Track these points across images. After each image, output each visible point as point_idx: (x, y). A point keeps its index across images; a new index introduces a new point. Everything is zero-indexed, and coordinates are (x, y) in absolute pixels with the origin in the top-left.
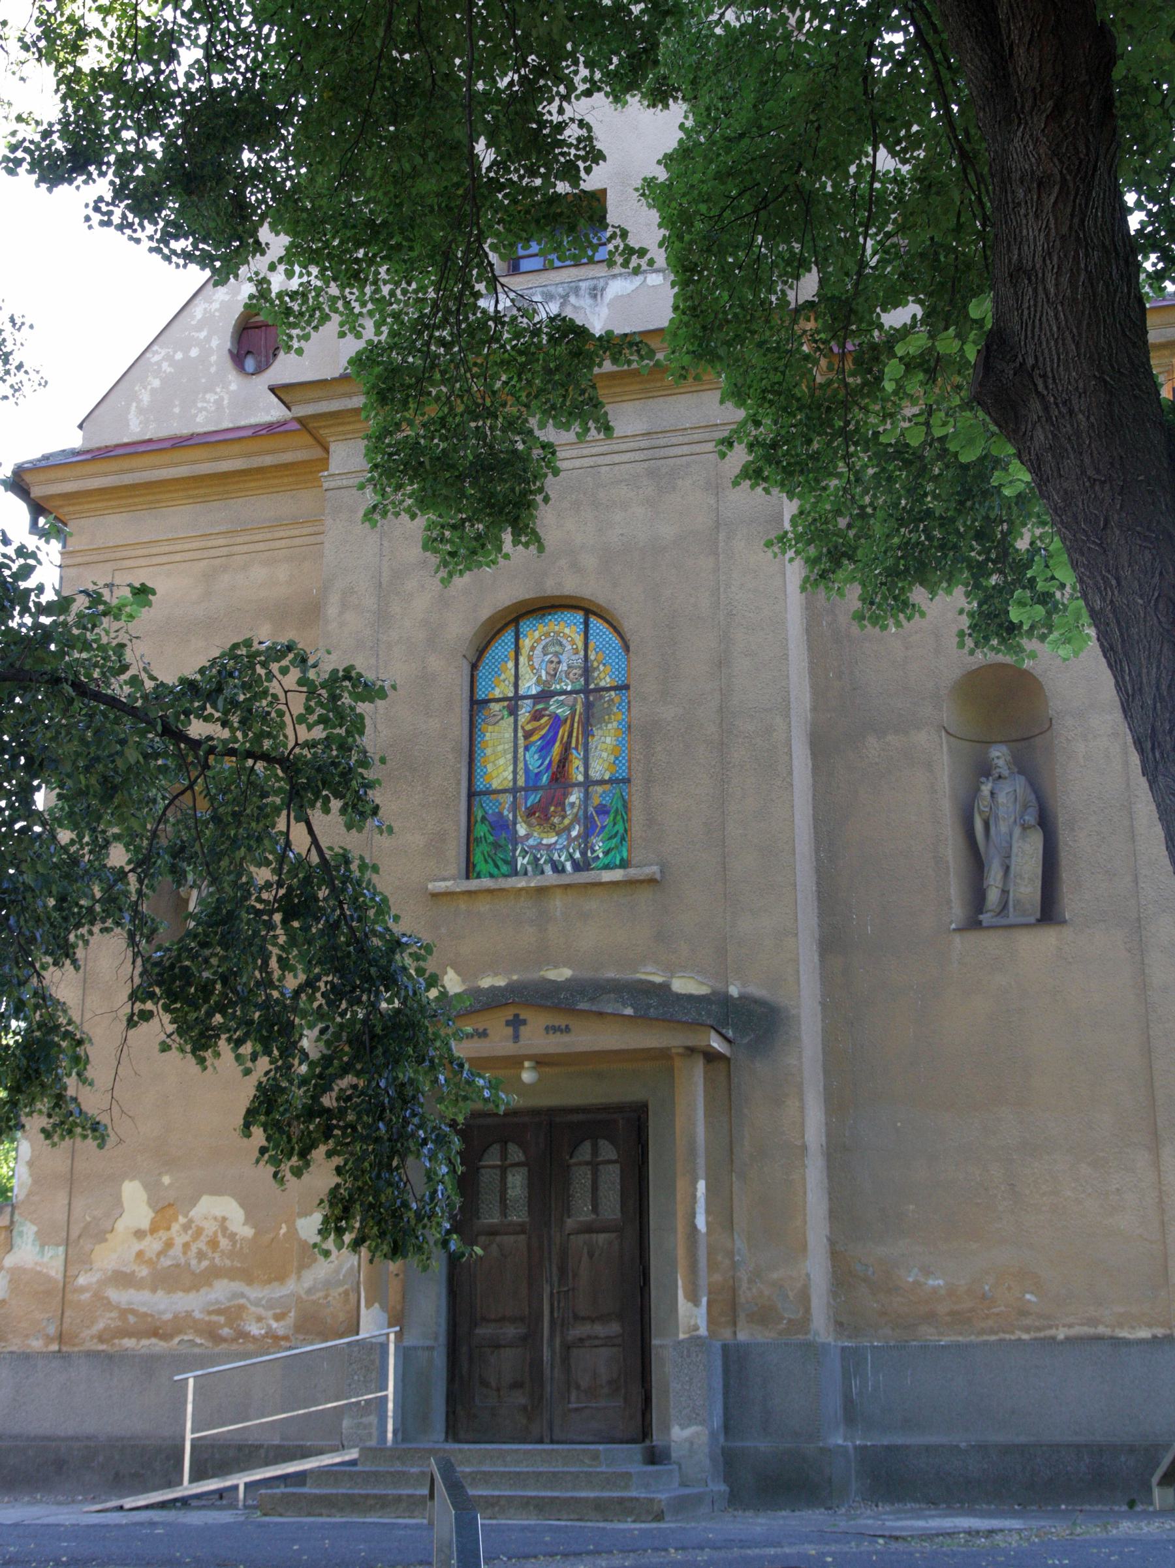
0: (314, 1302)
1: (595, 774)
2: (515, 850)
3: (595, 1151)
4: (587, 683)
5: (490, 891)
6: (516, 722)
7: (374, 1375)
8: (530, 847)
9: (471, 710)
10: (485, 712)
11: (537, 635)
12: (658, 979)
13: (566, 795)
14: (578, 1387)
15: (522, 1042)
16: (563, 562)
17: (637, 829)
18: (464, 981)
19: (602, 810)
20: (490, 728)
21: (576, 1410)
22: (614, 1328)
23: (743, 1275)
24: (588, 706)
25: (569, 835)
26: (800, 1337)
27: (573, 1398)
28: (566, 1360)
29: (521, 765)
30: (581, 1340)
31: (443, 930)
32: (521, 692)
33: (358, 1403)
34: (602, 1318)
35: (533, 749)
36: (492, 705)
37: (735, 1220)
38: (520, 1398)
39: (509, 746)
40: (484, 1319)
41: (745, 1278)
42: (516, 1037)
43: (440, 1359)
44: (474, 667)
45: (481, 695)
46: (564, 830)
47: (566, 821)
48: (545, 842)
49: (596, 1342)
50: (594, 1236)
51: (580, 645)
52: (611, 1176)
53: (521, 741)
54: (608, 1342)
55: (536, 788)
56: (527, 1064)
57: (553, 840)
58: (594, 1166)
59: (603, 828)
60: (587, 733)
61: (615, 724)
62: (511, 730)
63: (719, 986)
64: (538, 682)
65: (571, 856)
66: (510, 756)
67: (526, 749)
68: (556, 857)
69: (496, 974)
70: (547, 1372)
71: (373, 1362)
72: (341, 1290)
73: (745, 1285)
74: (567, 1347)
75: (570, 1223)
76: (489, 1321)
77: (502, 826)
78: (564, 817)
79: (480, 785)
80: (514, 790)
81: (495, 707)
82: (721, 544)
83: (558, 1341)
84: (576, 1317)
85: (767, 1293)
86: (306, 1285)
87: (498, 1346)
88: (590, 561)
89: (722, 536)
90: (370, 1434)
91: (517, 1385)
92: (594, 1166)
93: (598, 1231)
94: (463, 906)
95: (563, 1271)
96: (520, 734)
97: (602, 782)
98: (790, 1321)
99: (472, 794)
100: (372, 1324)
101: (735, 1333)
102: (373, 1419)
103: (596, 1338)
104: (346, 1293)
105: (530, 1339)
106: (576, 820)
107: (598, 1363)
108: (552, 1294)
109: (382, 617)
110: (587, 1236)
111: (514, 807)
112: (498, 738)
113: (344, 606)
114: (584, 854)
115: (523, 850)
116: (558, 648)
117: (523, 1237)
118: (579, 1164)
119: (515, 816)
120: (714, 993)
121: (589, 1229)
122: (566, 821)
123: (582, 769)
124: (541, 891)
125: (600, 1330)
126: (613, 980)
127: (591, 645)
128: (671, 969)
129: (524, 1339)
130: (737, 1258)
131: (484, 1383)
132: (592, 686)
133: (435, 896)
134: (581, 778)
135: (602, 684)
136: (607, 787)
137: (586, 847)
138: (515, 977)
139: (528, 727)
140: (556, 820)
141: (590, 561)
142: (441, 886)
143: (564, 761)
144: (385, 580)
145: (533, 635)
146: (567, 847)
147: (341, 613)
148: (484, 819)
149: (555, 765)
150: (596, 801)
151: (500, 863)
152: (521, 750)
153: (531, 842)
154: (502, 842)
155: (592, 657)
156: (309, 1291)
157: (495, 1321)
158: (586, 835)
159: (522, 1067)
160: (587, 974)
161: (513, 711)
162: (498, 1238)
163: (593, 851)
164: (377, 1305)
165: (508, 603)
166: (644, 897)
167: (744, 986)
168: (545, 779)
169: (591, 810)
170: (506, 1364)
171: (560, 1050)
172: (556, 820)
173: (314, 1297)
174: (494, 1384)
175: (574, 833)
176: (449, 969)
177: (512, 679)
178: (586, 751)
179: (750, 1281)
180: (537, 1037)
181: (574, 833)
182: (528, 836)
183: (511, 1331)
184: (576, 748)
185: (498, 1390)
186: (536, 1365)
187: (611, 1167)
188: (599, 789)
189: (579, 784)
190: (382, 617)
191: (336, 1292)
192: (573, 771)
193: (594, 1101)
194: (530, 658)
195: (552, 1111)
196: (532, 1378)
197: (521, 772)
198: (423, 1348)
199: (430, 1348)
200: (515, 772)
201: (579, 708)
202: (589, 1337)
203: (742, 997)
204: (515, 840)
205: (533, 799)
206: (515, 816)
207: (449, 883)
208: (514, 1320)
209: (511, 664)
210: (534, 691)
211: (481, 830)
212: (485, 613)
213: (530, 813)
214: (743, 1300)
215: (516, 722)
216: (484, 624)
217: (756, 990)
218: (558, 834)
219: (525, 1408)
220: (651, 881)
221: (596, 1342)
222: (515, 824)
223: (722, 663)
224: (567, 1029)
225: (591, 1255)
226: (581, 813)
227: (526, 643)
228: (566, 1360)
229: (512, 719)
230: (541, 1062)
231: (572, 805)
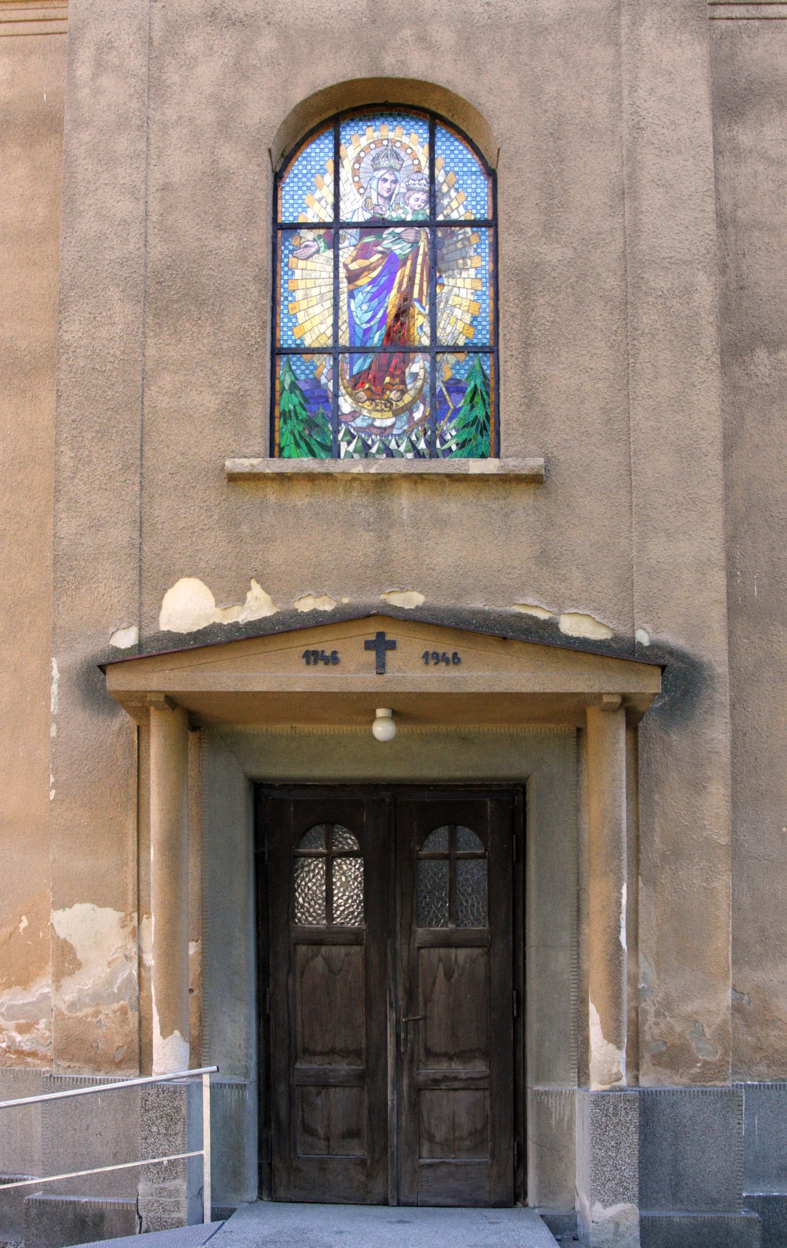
0: (79, 1021)
1: (445, 336)
2: (336, 432)
3: (453, 841)
4: (433, 213)
5: (311, 477)
6: (336, 257)
7: (179, 1127)
8: (358, 429)
9: (274, 237)
10: (295, 241)
11: (364, 142)
12: (543, 615)
13: (406, 363)
14: (431, 1139)
15: (388, 675)
16: (407, 33)
17: (509, 409)
18: (274, 602)
19: (455, 387)
20: (301, 264)
21: (430, 1166)
22: (479, 1068)
23: (649, 1006)
24: (434, 245)
25: (411, 417)
26: (717, 1083)
27: (425, 1152)
28: (415, 1106)
29: (344, 317)
30: (436, 1081)
31: (245, 529)
32: (344, 217)
33: (161, 1163)
34: (464, 1056)
35: (360, 297)
36: (303, 232)
37: (641, 936)
38: (358, 1152)
39: (328, 290)
40: (306, 1051)
41: (652, 1010)
42: (381, 667)
43: (251, 1097)
44: (278, 177)
45: (285, 217)
46: (403, 410)
47: (407, 398)
48: (377, 423)
49: (456, 1085)
50: (453, 951)
51: (424, 161)
52: (474, 874)
53: (344, 285)
54: (470, 1084)
55: (364, 351)
56: (380, 712)
57: (389, 422)
58: (451, 859)
59: (457, 411)
60: (433, 281)
61: (472, 272)
62: (330, 268)
63: (623, 630)
64: (365, 208)
65: (413, 446)
66: (329, 304)
67: (351, 295)
68: (393, 445)
69: (319, 595)
70: (392, 1119)
71: (177, 1110)
72: (116, 1006)
73: (651, 1019)
74: (417, 1089)
75: (421, 933)
76: (314, 1053)
77: (318, 398)
78: (403, 392)
79: (286, 340)
80: (334, 351)
81: (308, 235)
82: (624, 31)
83: (405, 1081)
84: (429, 1053)
85: (678, 1029)
86: (68, 998)
87: (326, 1086)
88: (444, 36)
89: (625, 20)
90: (177, 1203)
91: (352, 1134)
92: (451, 859)
93: (457, 946)
94: (272, 498)
95: (411, 994)
96: (342, 273)
97: (455, 349)
98: (706, 1063)
99: (276, 352)
100: (168, 1057)
101: (637, 1078)
102: (181, 1184)
103: (456, 1079)
104: (123, 1011)
105: (369, 1078)
106: (420, 396)
107: (456, 1109)
108: (398, 1021)
109: (154, 88)
110: (443, 951)
111: (336, 375)
112: (310, 276)
113: (99, 67)
114: (430, 444)
115: (348, 432)
116: (393, 162)
117: (357, 948)
118: (432, 857)
119: (336, 386)
120: (616, 638)
121: (448, 942)
122: (407, 398)
123: (427, 329)
124: (383, 481)
125: (459, 1069)
126: (482, 612)
127: (439, 162)
128: (558, 603)
129: (361, 1077)
130: (641, 986)
131: (308, 1130)
132: (440, 218)
133: (234, 478)
134: (426, 341)
135: (454, 216)
136: (461, 356)
137: (434, 437)
138: (346, 600)
139: (354, 266)
140: (393, 395)
141: (444, 36)
142: (244, 464)
143: (403, 313)
144: (157, 36)
145: (361, 139)
146: (407, 433)
147: (95, 76)
148: (294, 386)
149: (390, 320)
150: (447, 373)
151: (316, 449)
152: (344, 297)
153: (359, 422)
154: (319, 420)
155: (440, 176)
156: (72, 1006)
157: (322, 1054)
158: (433, 419)
159: (372, 719)
160: (444, 602)
161: (334, 244)
162: (324, 949)
163: (443, 442)
164: (177, 1033)
165: (330, 83)
166: (523, 501)
167: (655, 631)
168: (377, 339)
169: (440, 385)
170: (336, 1107)
171: (445, 689)
172: (393, 395)
173: (80, 1014)
174: (322, 1135)
175: (417, 415)
176: (253, 583)
177: (331, 199)
178: (433, 305)
179: (658, 1014)
180: (411, 670)
181: (417, 415)
182: (354, 414)
183: (343, 1068)
184: (420, 301)
185: (328, 1139)
186: (378, 1110)
187: (472, 864)
188: (451, 358)
189: (423, 350)
190: (154, 88)
191: (108, 1010)
192: (415, 331)
193: (458, 774)
194: (355, 172)
195: (396, 787)
196: (373, 1125)
197: (344, 327)
198: (231, 1086)
199: (241, 1087)
200: (336, 326)
201: (423, 246)
202: (446, 1078)
203: (654, 646)
204: (336, 418)
205: (361, 364)
206: (336, 386)
207: (255, 461)
208: (345, 1054)
209: (329, 178)
210: (362, 217)
211: (289, 402)
212: (299, 94)
213: (357, 382)
214: (648, 1037)
215: (336, 257)
216: (294, 111)
217: (672, 639)
218: (396, 414)
219: (362, 1162)
220: (535, 480)
221: (456, 1085)
222: (336, 396)
223: (625, 192)
224: (456, 660)
225: (448, 975)
226: (427, 388)
227: (349, 152)
228: (415, 1106)
229: (330, 253)
230: (403, 710)
231: (415, 376)
